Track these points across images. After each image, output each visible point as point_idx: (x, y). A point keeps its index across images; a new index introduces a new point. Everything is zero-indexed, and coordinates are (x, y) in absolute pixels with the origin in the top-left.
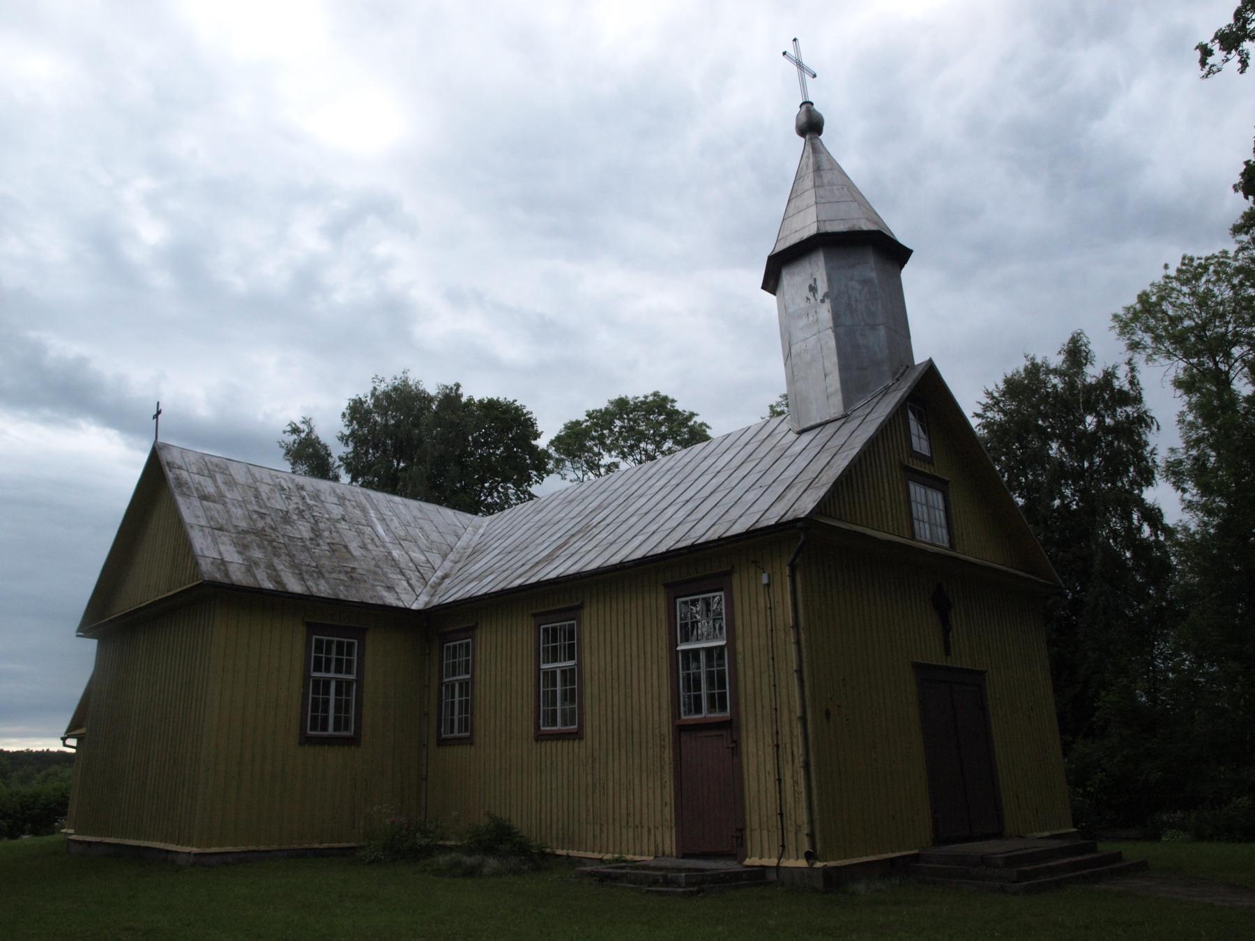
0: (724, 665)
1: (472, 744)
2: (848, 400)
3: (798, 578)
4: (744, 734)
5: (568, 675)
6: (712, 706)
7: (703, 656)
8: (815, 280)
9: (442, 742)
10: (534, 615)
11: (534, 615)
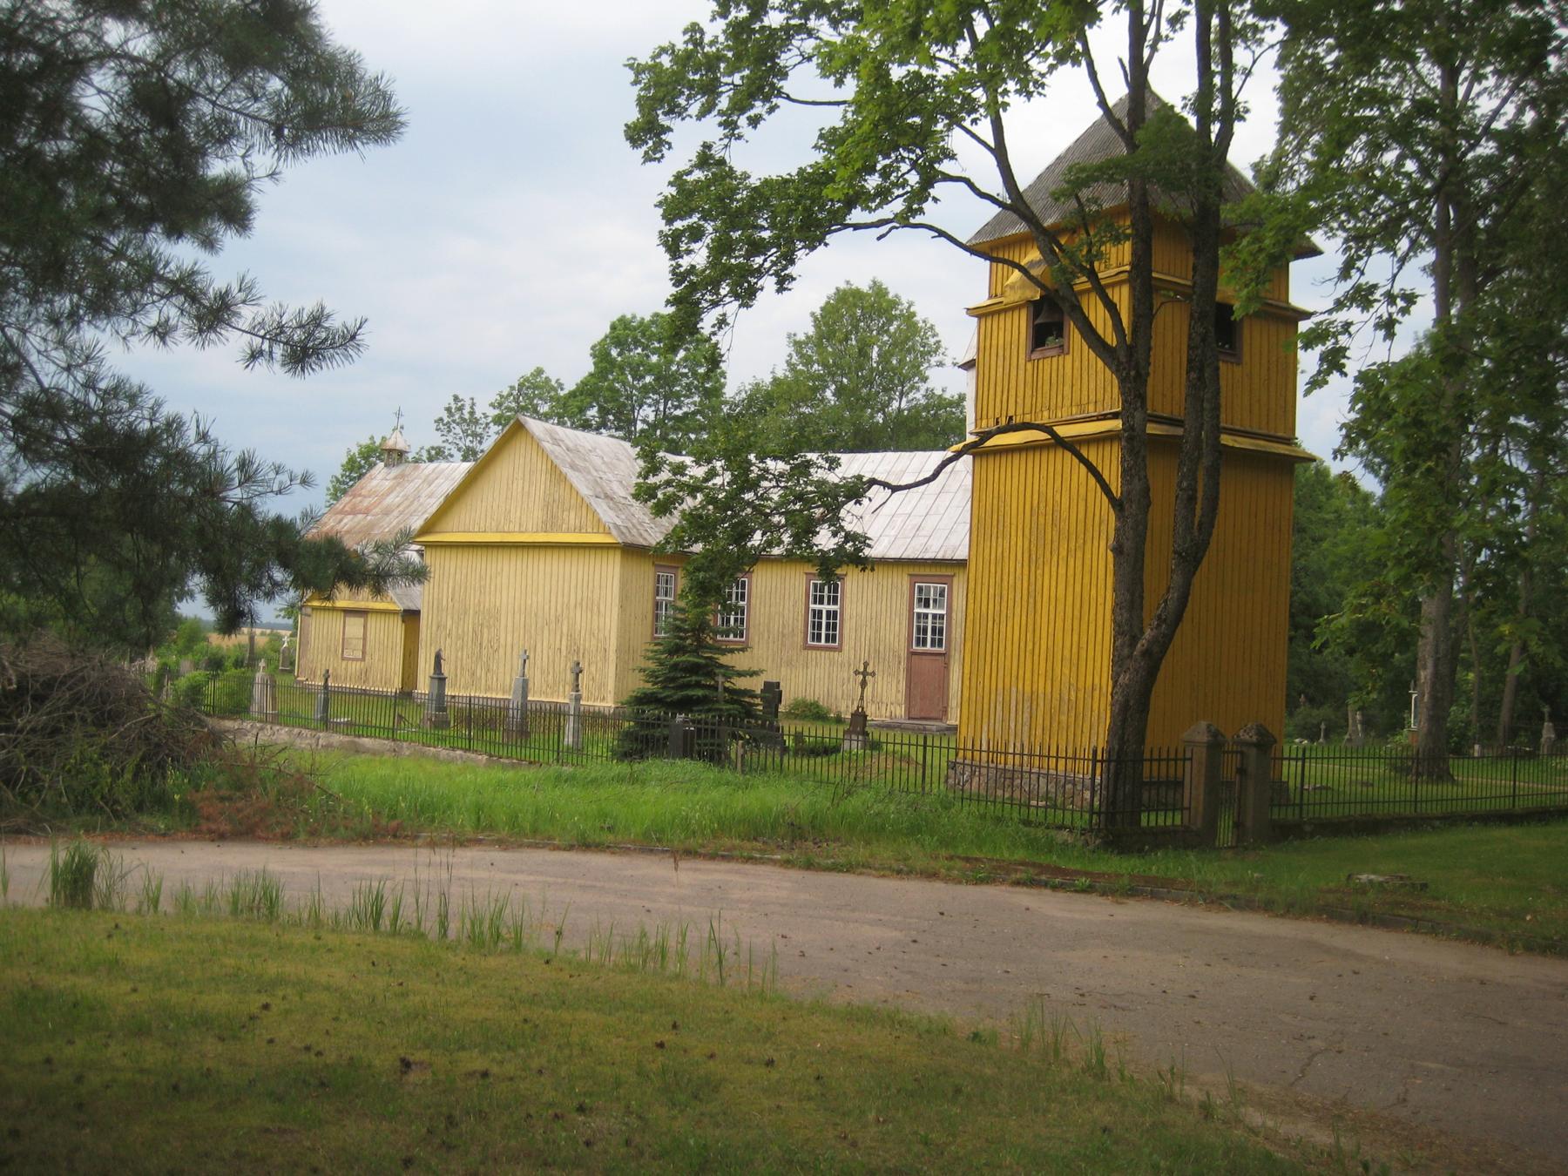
7: (930, 617)
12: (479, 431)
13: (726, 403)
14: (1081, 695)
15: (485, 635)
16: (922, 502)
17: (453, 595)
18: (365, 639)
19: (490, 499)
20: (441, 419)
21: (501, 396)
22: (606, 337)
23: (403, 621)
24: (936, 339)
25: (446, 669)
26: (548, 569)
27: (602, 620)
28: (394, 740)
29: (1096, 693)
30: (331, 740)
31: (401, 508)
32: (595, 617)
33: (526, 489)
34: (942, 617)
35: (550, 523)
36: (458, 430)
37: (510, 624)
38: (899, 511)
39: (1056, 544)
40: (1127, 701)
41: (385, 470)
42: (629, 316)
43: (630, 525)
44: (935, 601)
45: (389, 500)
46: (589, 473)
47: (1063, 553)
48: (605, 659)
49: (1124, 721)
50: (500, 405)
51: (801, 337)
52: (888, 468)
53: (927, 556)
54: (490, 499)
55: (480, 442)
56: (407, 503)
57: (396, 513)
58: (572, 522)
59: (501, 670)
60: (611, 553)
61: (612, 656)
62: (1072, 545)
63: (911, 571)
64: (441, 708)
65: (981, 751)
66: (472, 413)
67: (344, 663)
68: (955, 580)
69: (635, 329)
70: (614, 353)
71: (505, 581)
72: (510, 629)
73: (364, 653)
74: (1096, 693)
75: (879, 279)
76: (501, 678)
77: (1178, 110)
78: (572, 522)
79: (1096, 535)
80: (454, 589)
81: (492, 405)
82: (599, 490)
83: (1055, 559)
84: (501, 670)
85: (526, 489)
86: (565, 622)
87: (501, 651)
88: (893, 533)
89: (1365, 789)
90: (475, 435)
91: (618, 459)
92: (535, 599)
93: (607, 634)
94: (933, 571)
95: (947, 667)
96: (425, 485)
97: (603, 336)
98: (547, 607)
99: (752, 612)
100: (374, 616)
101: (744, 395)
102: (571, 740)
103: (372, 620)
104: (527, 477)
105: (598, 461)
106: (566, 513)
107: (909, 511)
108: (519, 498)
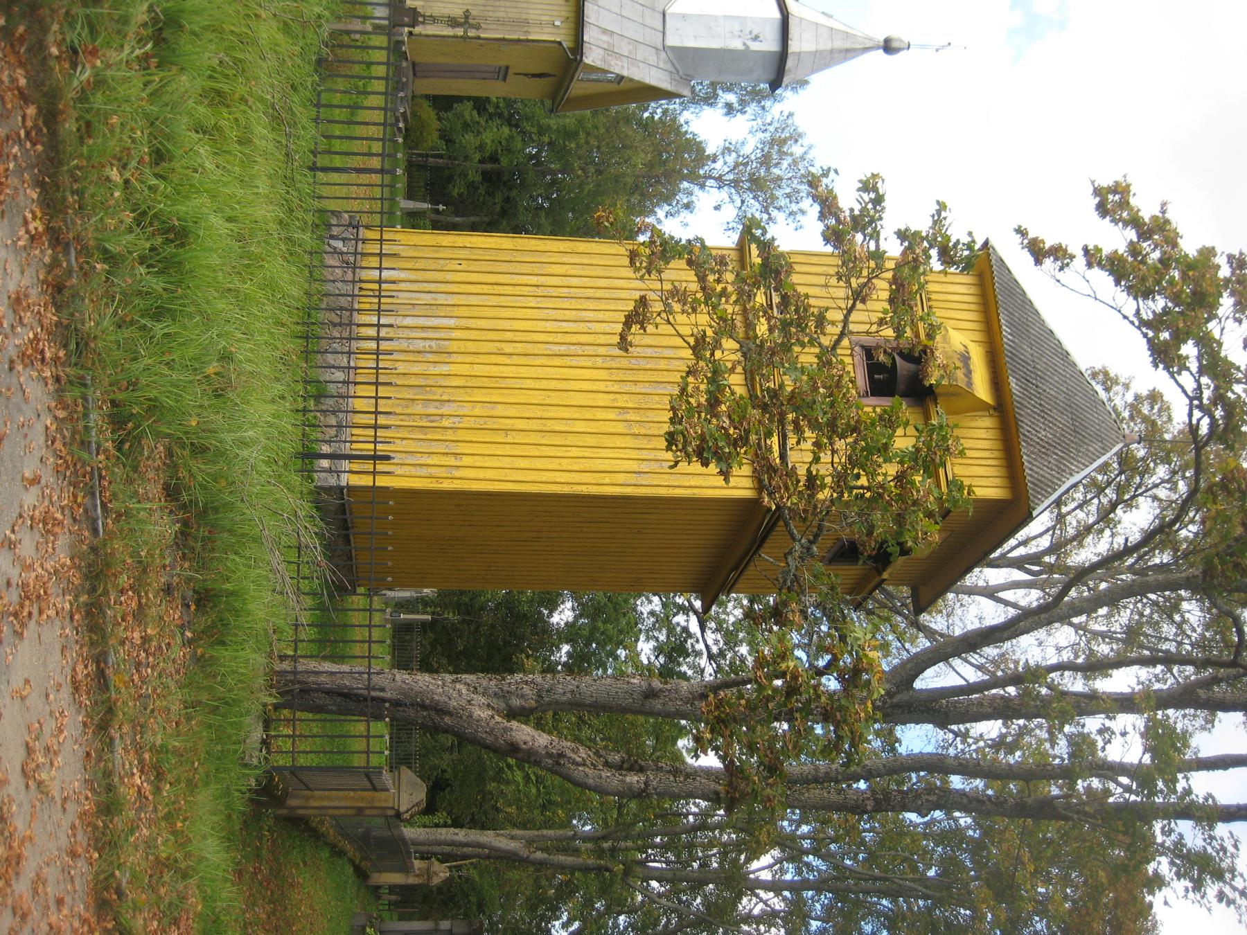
2: (673, 48)
14: (449, 435)
29: (451, 461)
39: (633, 389)
40: (450, 714)
47: (622, 401)
49: (423, 707)
62: (632, 416)
65: (374, 473)
74: (451, 461)
77: (1093, 736)
79: (645, 454)
83: (616, 388)
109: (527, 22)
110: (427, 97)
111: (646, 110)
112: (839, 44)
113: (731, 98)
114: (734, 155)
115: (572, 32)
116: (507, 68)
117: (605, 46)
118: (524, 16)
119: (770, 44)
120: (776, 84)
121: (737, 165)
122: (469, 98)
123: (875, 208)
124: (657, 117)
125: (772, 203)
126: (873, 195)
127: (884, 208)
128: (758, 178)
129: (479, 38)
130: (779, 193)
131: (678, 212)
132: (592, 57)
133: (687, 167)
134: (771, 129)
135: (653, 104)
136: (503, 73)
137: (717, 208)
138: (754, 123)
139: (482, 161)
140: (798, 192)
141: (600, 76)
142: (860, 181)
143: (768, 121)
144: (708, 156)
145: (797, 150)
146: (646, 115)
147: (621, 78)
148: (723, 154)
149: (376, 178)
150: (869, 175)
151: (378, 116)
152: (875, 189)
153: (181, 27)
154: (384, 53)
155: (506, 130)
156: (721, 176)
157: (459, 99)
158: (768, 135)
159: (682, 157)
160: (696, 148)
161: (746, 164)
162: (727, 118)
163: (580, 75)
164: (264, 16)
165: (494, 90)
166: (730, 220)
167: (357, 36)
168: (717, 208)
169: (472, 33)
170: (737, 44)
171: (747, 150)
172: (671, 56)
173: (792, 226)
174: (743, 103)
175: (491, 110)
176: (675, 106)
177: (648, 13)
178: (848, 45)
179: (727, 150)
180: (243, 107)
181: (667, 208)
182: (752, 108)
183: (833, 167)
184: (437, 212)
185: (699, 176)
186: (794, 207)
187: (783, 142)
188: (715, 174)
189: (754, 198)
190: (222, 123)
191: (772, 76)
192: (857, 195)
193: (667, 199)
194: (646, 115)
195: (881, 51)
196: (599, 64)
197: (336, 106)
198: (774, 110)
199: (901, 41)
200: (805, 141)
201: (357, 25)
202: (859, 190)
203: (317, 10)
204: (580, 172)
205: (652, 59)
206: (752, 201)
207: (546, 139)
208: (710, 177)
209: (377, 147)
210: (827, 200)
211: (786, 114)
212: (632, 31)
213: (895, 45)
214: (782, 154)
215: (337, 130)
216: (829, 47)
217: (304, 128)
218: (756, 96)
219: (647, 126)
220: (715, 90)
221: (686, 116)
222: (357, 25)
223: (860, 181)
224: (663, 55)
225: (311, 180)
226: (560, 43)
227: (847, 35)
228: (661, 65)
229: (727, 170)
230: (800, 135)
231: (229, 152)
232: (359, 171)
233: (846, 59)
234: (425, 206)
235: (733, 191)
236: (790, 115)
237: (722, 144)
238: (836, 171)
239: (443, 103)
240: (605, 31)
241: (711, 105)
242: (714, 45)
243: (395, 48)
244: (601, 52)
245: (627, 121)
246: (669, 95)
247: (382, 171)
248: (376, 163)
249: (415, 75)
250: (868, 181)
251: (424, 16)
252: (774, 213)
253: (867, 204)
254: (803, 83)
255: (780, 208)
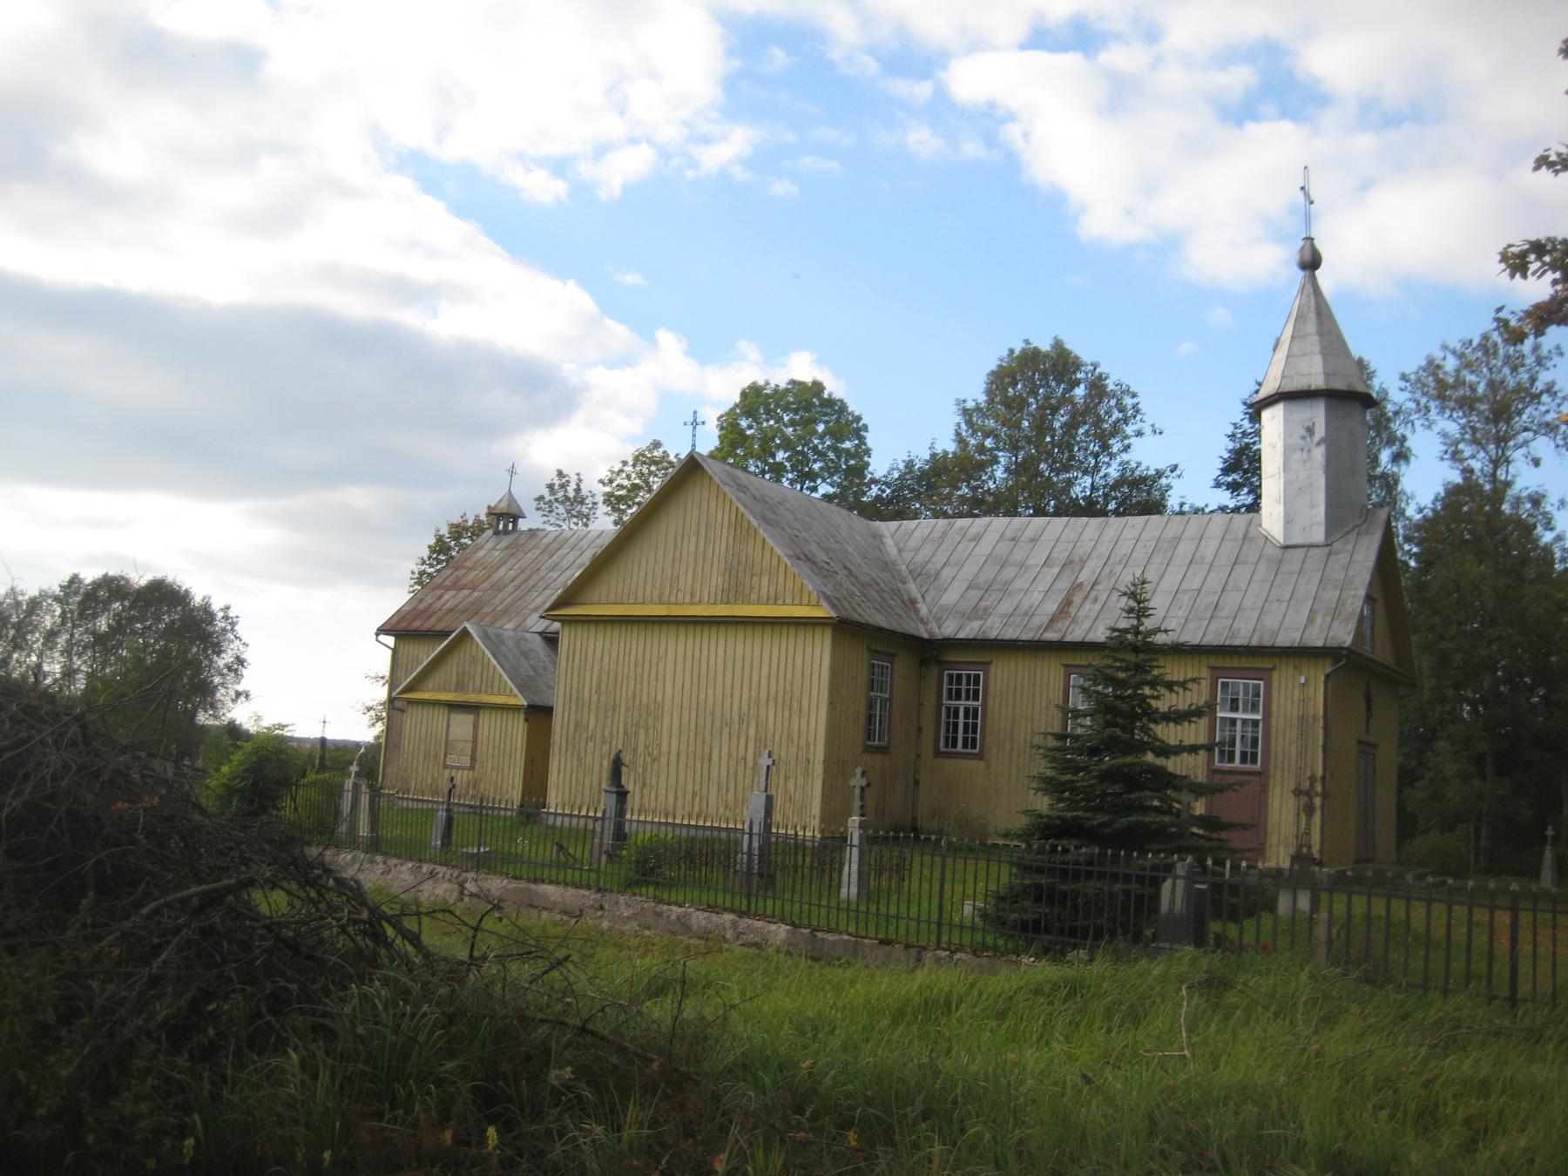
0: (1258, 732)
1: (888, 753)
2: (1328, 533)
3: (1330, 686)
4: (1271, 782)
5: (872, 690)
6: (1244, 759)
7: (1239, 724)
8: (1314, 424)
9: (938, 754)
10: (1065, 665)
11: (1065, 665)
12: (585, 510)
13: (874, 481)
15: (642, 738)
16: (1213, 575)
17: (599, 685)
18: (475, 741)
19: (651, 562)
20: (541, 498)
21: (612, 472)
22: (736, 406)
23: (526, 720)
24: (1135, 401)
25: (628, 781)
26: (730, 652)
27: (805, 721)
28: (599, 890)
30: (486, 886)
31: (516, 583)
32: (795, 717)
33: (701, 547)
34: (1255, 723)
35: (734, 592)
36: (561, 510)
37: (676, 724)
38: (1185, 586)
41: (494, 539)
42: (761, 383)
43: (840, 596)
44: (1245, 703)
45: (500, 573)
46: (783, 529)
48: (807, 774)
50: (611, 481)
51: (970, 405)
52: (1157, 534)
53: (1237, 642)
54: (651, 562)
55: (586, 525)
56: (523, 577)
57: (510, 588)
58: (764, 591)
59: (663, 784)
60: (818, 631)
61: (819, 770)
63: (1213, 662)
64: (620, 835)
66: (578, 490)
67: (447, 772)
68: (1275, 675)
69: (768, 396)
70: (744, 423)
71: (670, 666)
72: (675, 732)
73: (473, 760)
75: (1060, 337)
76: (662, 792)
78: (764, 591)
80: (600, 676)
81: (601, 481)
82: (798, 551)
84: (663, 784)
85: (701, 547)
86: (753, 724)
87: (663, 760)
88: (1181, 613)
89: (398, 852)
90: (580, 515)
91: (812, 518)
92: (711, 692)
93: (811, 739)
94: (1244, 662)
95: (1264, 790)
96: (546, 556)
97: (731, 406)
98: (727, 703)
99: (989, 716)
100: (488, 712)
101: (896, 475)
102: (854, 890)
103: (486, 719)
104: (703, 531)
105: (790, 517)
106: (755, 579)
107: (1196, 585)
108: (692, 561)
109: (1302, 718)
110: (1399, 845)
111: (1406, 564)
112: (1311, 327)
113: (1385, 456)
114: (1461, 446)
115: (579, 627)
116: (1360, 742)
117: (1329, 619)
118: (1295, 722)
119: (1317, 413)
120: (1366, 401)
121: (1475, 441)
122: (1400, 792)
123: (1549, 252)
124: (1415, 550)
125: (1526, 390)
126: (1532, 257)
127: (1549, 239)
128: (1492, 411)
129: (1323, 778)
130: (1511, 383)
131: (1545, 514)
132: (1344, 635)
133: (1481, 507)
134: (1423, 400)
135: (1399, 554)
136: (1367, 748)
137: (1536, 462)
138: (1417, 423)
139: (1483, 777)
140: (1507, 357)
141: (1367, 625)
142: (1512, 276)
143: (1412, 405)
144: (1465, 479)
145: (1451, 364)
146: (1412, 563)
147: (1369, 599)
148: (1462, 461)
149: (1525, 917)
150: (1503, 266)
151: (1419, 909)
152: (1523, 255)
153: (1340, 1152)
154: (1355, 898)
155: (1441, 745)
156: (1491, 461)
157: (1401, 805)
158: (1432, 405)
159: (1470, 513)
160: (1453, 496)
161: (1474, 429)
162: (1412, 459)
163: (1366, 650)
164: (1316, 1047)
165: (1389, 758)
166: (1552, 444)
167: (1334, 931)
168: (1536, 462)
169: (1319, 789)
170: (1319, 454)
171: (1453, 428)
172: (1337, 535)
173: (1556, 360)
174: (1391, 440)
175: (1414, 763)
176: (1400, 528)
177: (1285, 568)
178: (1312, 315)
179: (1456, 456)
180: (1437, 1086)
181: (1539, 528)
182: (1398, 428)
183: (1493, 314)
184: (1556, 839)
185: (1494, 490)
186: (1530, 360)
187: (1442, 385)
188: (1489, 469)
189: (1520, 413)
190: (1460, 1113)
191: (1357, 408)
192: (1531, 279)
193: (1527, 529)
194: (1412, 563)
195: (1318, 272)
196: (1352, 627)
197: (1447, 967)
198: (1398, 397)
199: (1302, 249)
200: (1438, 354)
201: (1321, 932)
202: (1524, 276)
203: (1304, 977)
204: (1494, 647)
205: (1343, 559)
206: (1524, 417)
207: (1450, 692)
208: (1494, 474)
209: (1460, 912)
210: (1541, 318)
211: (1403, 384)
212: (1309, 587)
213: (1308, 256)
214: (1459, 383)
215: (1457, 965)
216: (1316, 339)
217: (1458, 1009)
218: (1382, 424)
219: (1426, 561)
220: (1376, 477)
221: (1411, 511)
222: (1321, 932)
223: (1512, 276)
224: (1337, 546)
225: (1530, 1005)
226: (1327, 677)
227: (1300, 318)
228: (1350, 547)
229: (1482, 454)
230: (1430, 362)
231: (1501, 1113)
232: (1514, 940)
233: (1330, 316)
234: (1548, 853)
235: (1511, 443)
236: (1404, 377)
237: (1447, 463)
238: (1499, 310)
239: (1407, 826)
240: (1310, 620)
241: (1396, 482)
242: (1321, 482)
243: (1340, 883)
244: (1336, 625)
245: (1422, 587)
246: (1388, 534)
247: (1514, 910)
248: (1503, 919)
249: (1372, 860)
250: (1509, 266)
251: (1300, 847)
252: (1539, 385)
253: (1544, 264)
254: (1361, 365)
255: (1533, 380)
